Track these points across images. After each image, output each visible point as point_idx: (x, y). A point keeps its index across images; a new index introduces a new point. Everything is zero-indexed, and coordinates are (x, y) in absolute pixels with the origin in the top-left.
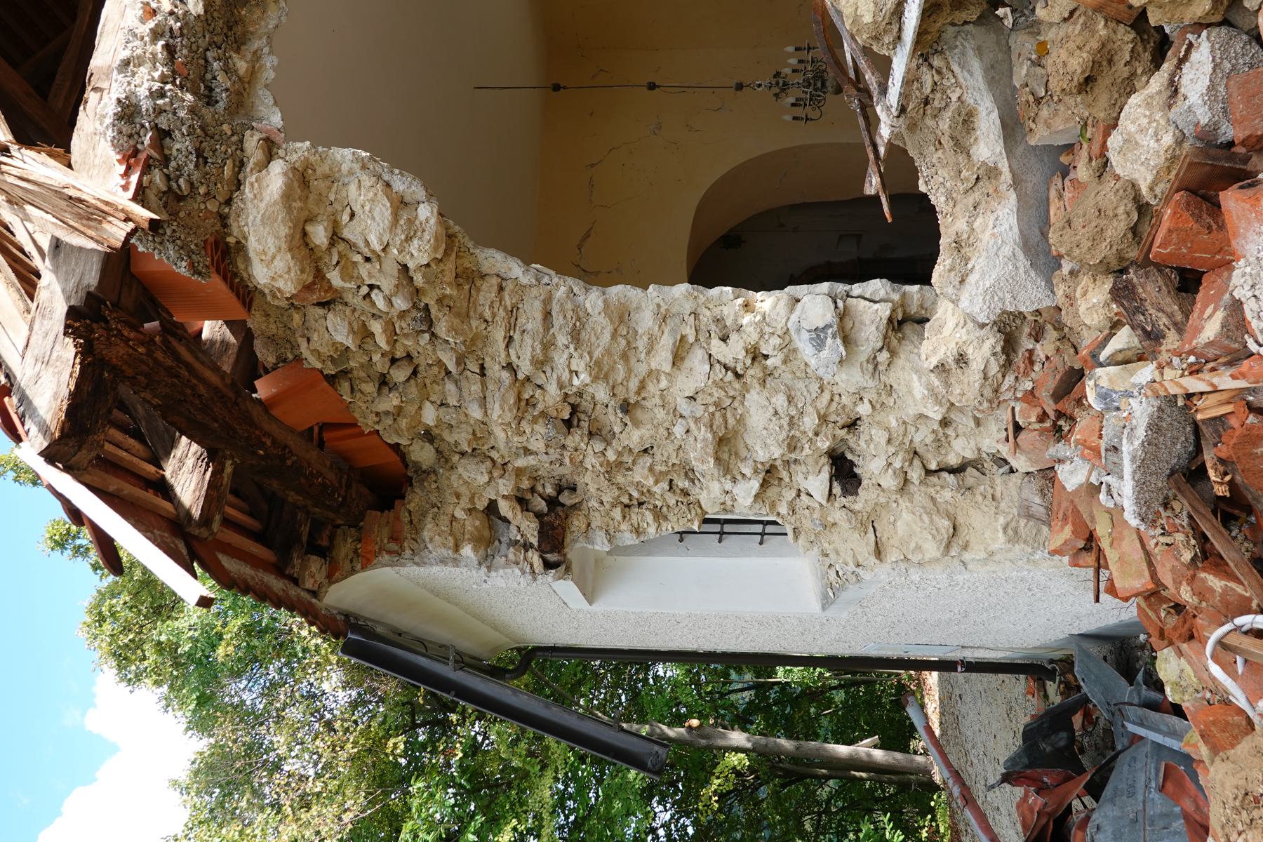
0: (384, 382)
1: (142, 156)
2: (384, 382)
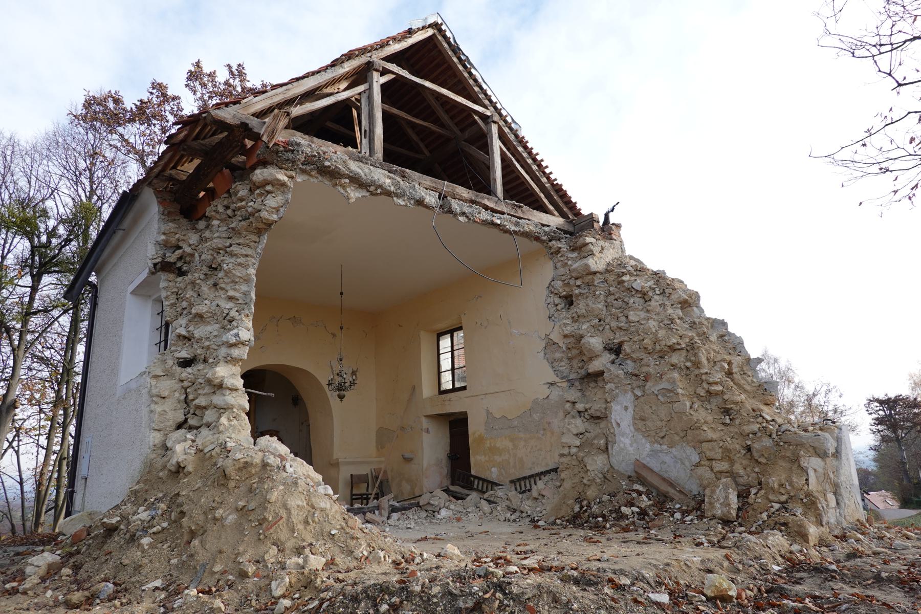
0: (227, 207)
1: (287, 146)
2: (227, 207)
